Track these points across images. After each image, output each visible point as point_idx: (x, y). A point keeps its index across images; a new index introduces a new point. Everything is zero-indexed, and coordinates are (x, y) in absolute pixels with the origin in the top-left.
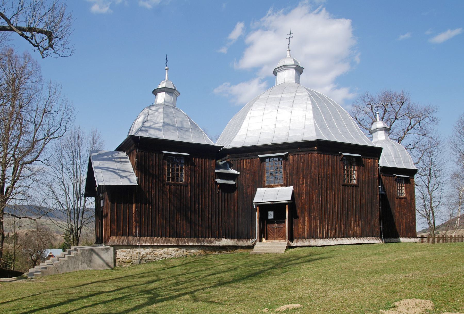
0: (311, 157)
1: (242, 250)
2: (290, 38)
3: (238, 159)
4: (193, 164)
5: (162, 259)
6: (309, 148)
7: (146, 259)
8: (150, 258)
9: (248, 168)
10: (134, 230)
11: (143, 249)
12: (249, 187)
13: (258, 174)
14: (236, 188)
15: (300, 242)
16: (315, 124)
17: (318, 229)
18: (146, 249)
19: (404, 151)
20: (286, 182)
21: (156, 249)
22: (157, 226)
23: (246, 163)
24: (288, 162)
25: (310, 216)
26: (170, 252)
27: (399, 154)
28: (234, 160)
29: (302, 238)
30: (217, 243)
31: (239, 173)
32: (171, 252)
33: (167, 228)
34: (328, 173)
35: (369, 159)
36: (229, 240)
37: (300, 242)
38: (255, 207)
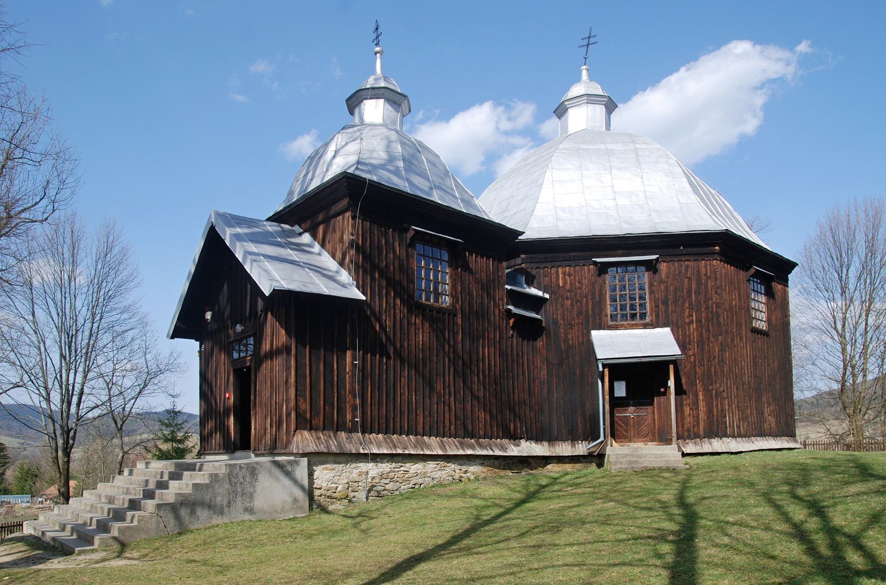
0: (705, 267)
1: (560, 465)
2: (588, 45)
4: (466, 267)
5: (412, 488)
6: (702, 249)
7: (380, 488)
8: (387, 487)
10: (349, 417)
11: (372, 464)
12: (571, 328)
14: (543, 329)
15: (690, 444)
17: (727, 418)
18: (380, 464)
20: (654, 317)
21: (400, 464)
22: (399, 406)
23: (562, 275)
25: (706, 390)
26: (430, 471)
28: (535, 268)
30: (514, 451)
32: (432, 472)
33: (418, 412)
35: (779, 283)
36: (533, 444)
38: (601, 369)
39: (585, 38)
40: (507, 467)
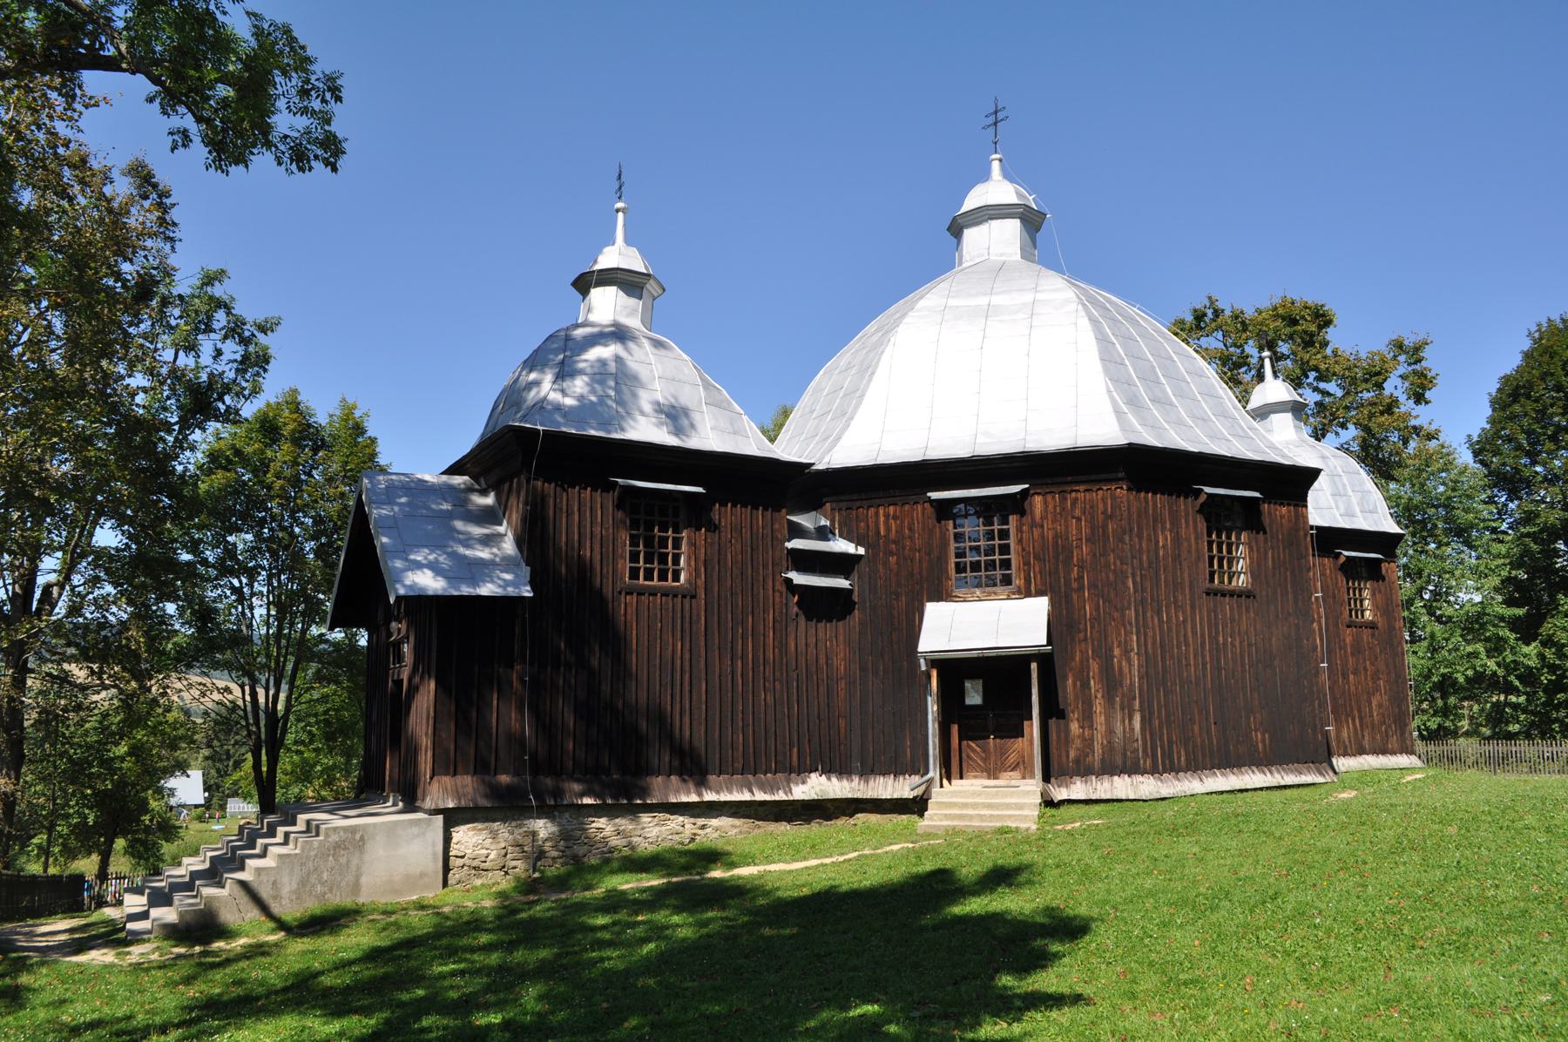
2: (995, 124)
3: (858, 504)
9: (893, 535)
13: (929, 554)
15: (1078, 783)
16: (1109, 391)
19: (1359, 474)
23: (883, 517)
24: (1025, 519)
27: (1344, 485)
29: (1084, 770)
31: (861, 551)
34: (1161, 553)
36: (834, 780)
37: (1078, 783)
38: (923, 668)
39: (991, 114)
40: (1393, 742)
